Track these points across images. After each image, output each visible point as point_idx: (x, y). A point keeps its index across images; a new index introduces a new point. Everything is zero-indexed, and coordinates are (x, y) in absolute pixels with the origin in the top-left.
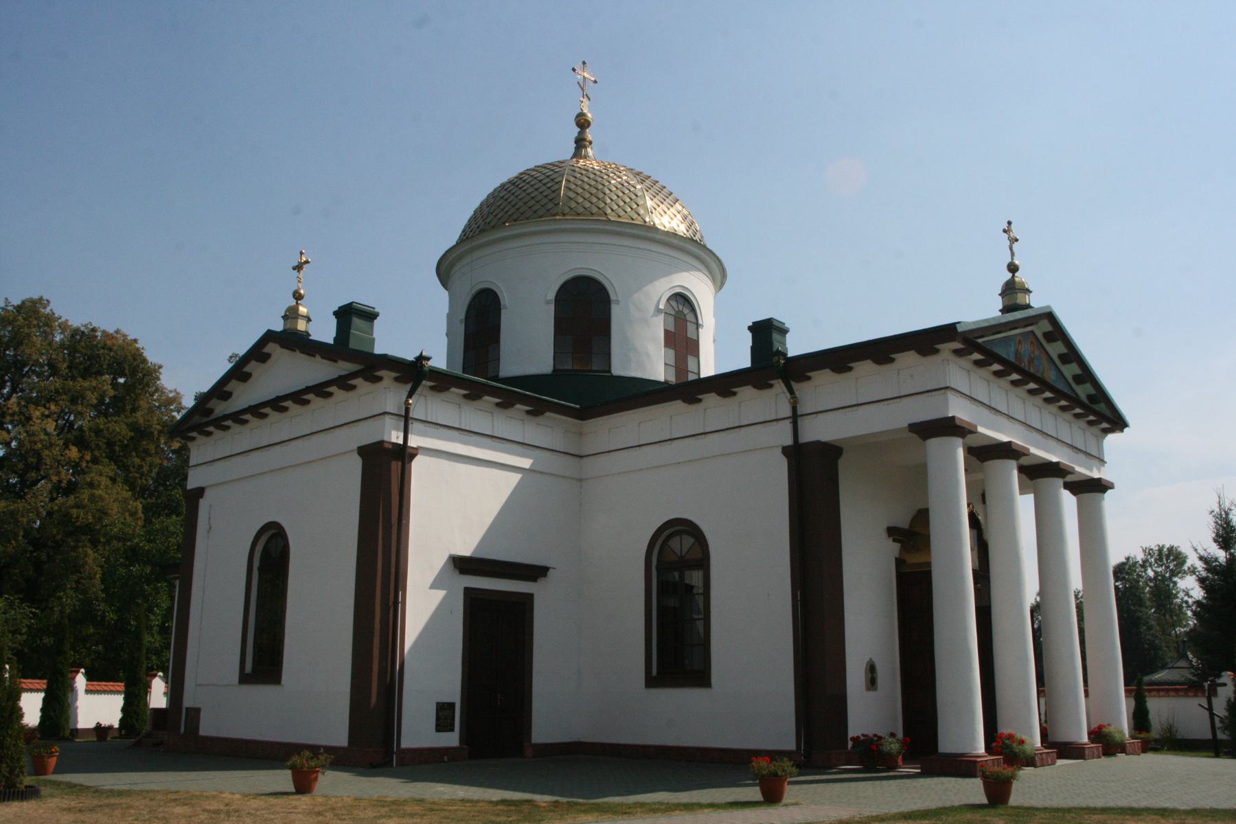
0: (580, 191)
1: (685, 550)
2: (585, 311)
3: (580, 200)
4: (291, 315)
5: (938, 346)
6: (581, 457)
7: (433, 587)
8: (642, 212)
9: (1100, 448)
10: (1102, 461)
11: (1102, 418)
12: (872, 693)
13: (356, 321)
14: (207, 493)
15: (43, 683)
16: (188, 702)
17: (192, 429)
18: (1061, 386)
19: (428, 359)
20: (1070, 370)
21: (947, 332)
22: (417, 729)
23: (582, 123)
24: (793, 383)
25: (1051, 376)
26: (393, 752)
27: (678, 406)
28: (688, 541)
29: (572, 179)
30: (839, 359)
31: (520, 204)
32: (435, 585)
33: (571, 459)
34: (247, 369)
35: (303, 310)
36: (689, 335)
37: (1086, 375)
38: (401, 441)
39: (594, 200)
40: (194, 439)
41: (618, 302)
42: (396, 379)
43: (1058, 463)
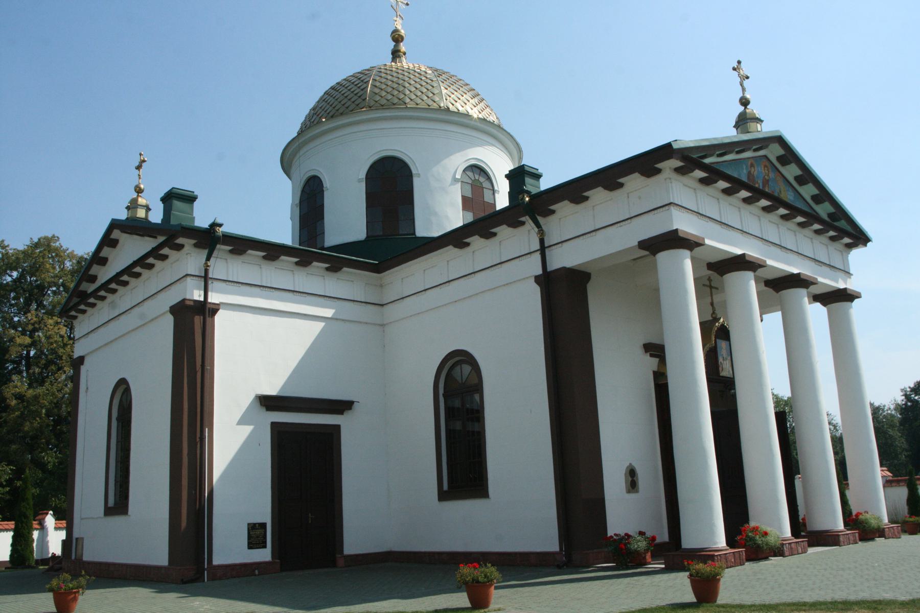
0: (383, 87)
1: (464, 378)
2: (391, 184)
3: (384, 94)
4: (133, 205)
5: (659, 166)
6: (382, 305)
7: (241, 422)
8: (437, 99)
9: (845, 261)
10: (848, 273)
11: (842, 233)
12: (633, 496)
13: (177, 204)
14: (86, 361)
15: (12, 524)
16: (76, 534)
17: (71, 309)
18: (799, 205)
19: (220, 225)
20: (808, 191)
21: (665, 151)
22: (229, 546)
23: (397, 38)
24: (539, 218)
25: (789, 197)
26: (204, 569)
27: (450, 251)
28: (467, 369)
29: (378, 78)
30: (575, 190)
31: (336, 103)
32: (242, 422)
33: (377, 307)
34: (102, 254)
35: (141, 201)
36: (486, 199)
37: (824, 195)
38: (202, 299)
39: (395, 93)
40: (75, 317)
41: (419, 175)
42: (196, 246)
43: (799, 274)
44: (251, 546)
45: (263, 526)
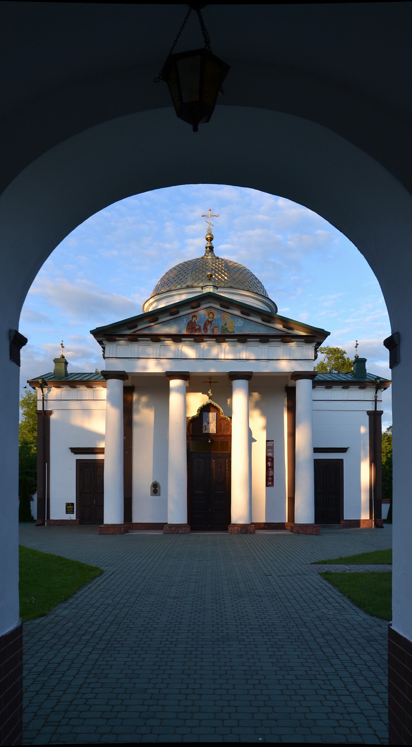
12: (156, 497)
22: (58, 512)
44: (67, 512)
45: (72, 504)
